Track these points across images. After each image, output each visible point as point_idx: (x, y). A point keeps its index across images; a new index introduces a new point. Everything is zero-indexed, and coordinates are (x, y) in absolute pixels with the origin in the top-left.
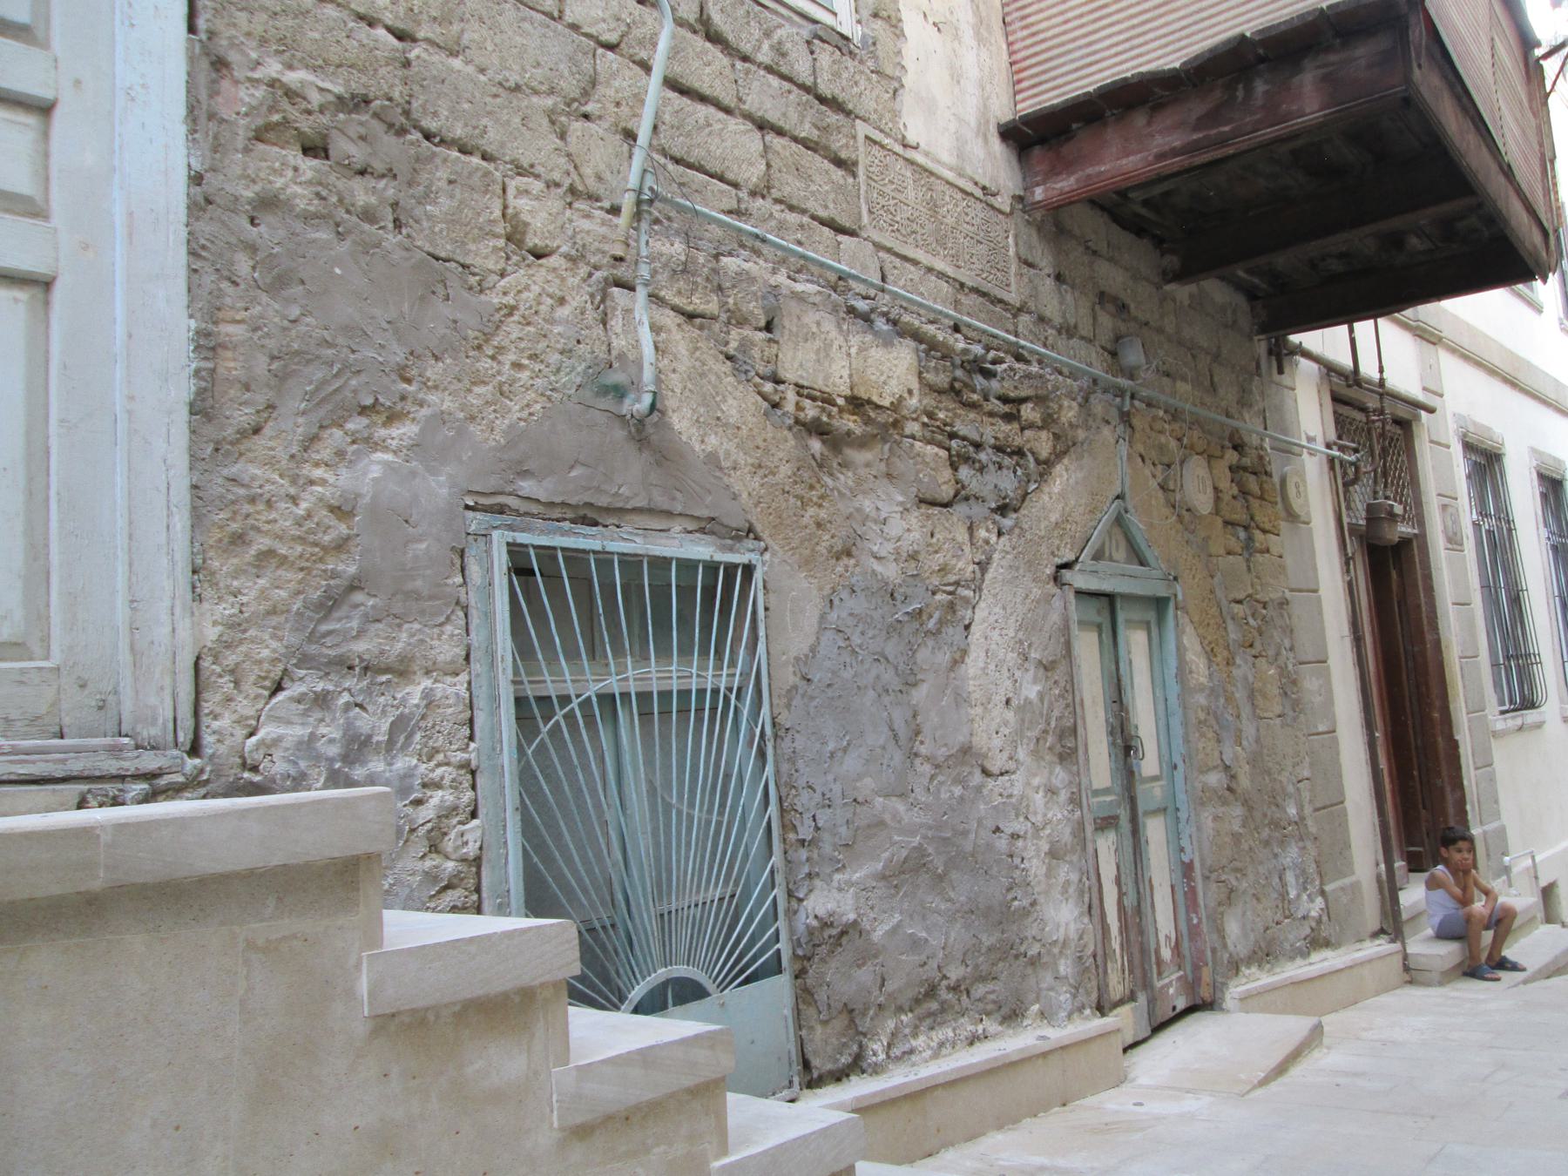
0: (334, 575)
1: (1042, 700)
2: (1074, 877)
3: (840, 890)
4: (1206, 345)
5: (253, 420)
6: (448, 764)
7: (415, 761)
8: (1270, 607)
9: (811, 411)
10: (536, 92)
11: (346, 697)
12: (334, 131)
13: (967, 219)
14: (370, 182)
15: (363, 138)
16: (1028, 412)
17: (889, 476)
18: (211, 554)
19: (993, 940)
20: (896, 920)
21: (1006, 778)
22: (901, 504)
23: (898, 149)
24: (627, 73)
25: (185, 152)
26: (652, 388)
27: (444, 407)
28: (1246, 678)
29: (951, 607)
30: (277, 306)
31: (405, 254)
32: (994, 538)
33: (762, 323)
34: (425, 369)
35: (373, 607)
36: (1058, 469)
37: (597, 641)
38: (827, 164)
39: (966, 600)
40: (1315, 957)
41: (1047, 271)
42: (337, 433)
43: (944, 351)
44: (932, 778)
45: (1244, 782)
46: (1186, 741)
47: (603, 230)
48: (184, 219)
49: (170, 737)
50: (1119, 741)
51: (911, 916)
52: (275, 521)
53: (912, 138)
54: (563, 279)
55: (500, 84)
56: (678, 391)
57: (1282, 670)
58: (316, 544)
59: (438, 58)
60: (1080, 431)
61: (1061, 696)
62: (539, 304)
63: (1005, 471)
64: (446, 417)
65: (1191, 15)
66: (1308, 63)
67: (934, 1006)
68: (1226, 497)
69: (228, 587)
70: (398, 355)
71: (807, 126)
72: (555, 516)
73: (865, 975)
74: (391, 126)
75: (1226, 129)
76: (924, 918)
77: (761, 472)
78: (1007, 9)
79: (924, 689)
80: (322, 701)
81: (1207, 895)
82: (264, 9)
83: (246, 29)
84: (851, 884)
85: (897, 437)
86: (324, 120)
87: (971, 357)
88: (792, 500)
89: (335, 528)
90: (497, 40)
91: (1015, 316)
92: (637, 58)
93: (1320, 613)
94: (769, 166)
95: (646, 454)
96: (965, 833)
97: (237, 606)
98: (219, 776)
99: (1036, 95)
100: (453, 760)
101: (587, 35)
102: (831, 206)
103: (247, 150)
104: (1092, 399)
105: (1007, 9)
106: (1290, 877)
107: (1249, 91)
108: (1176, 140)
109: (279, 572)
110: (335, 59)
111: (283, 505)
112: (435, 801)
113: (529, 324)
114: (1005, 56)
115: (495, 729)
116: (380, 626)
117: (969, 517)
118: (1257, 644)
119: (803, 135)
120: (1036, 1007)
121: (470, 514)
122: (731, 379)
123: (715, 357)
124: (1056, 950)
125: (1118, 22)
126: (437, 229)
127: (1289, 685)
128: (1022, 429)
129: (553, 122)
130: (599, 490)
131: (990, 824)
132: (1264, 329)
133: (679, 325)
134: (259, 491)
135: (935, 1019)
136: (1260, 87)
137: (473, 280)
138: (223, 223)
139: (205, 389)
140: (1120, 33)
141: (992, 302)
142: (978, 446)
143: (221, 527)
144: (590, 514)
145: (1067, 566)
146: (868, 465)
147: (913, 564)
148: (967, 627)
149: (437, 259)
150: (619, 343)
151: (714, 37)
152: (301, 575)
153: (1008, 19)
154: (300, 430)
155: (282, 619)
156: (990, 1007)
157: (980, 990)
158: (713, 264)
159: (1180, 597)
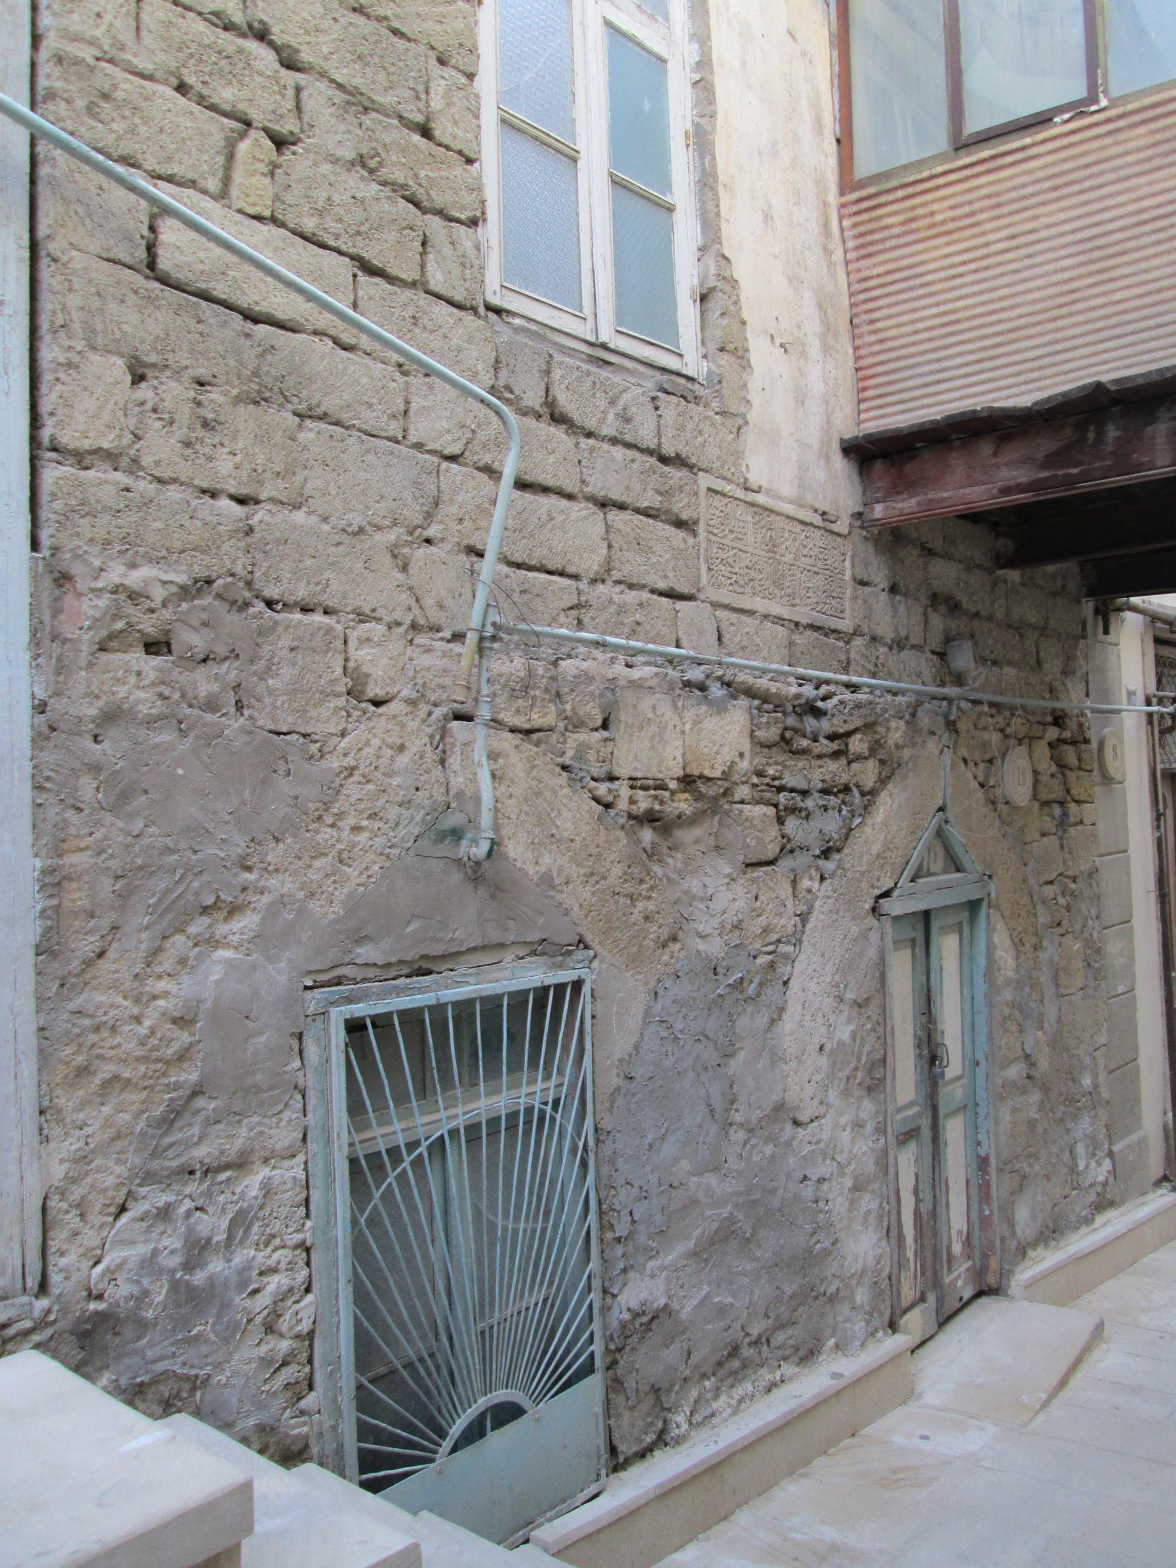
0: (177, 1086)
1: (854, 1039)
2: (874, 1205)
3: (652, 1276)
4: (1033, 620)
5: (97, 947)
6: (284, 1247)
7: (253, 1252)
8: (1080, 880)
9: (644, 802)
10: (379, 528)
11: (188, 1204)
12: (177, 624)
13: (805, 552)
14: (213, 668)
15: (205, 624)
16: (857, 744)
17: (717, 848)
18: (58, 1091)
19: (794, 1287)
20: (703, 1293)
21: (815, 1124)
22: (728, 875)
23: (740, 494)
24: (471, 484)
25: (28, 681)
26: (491, 834)
27: (285, 890)
28: (1052, 961)
29: (772, 966)
30: (120, 824)
31: (247, 738)
32: (816, 885)
33: (599, 723)
34: (267, 854)
35: (214, 1110)
36: (884, 795)
37: (428, 1081)
38: (670, 530)
39: (786, 956)
40: (1100, 1220)
41: (881, 586)
42: (179, 939)
43: (777, 702)
44: (746, 1143)
45: (1044, 1065)
46: (990, 1038)
47: (443, 663)
48: (28, 753)
49: (19, 1285)
50: (926, 1052)
51: (719, 1286)
52: (120, 1045)
53: (754, 479)
54: (403, 725)
55: (343, 530)
56: (514, 817)
57: (1089, 943)
58: (159, 1060)
59: (284, 515)
60: (906, 750)
61: (874, 1030)
62: (379, 757)
63: (830, 812)
64: (286, 899)
65: (1045, 345)
66: (1163, 413)
67: (735, 1364)
68: (1044, 779)
69: (73, 1122)
70: (239, 844)
71: (650, 493)
72: (390, 976)
73: (673, 1353)
74: (233, 603)
75: (1075, 471)
76: (731, 1283)
77: (592, 880)
78: (855, 310)
79: (741, 1056)
80: (165, 1213)
81: (999, 1187)
82: (106, 509)
83: (90, 536)
84: (662, 1268)
85: (726, 807)
86: (166, 614)
87: (803, 701)
88: (622, 900)
89: (178, 1039)
90: (341, 482)
91: (847, 643)
92: (481, 464)
93: (1128, 873)
94: (610, 546)
95: (482, 892)
96: (773, 1191)
97: (83, 1140)
98: (66, 1314)
99: (880, 407)
100: (289, 1243)
101: (430, 452)
102: (671, 574)
103: (91, 666)
104: (920, 713)
105: (855, 310)
106: (1080, 1150)
107: (1100, 433)
108: (1022, 475)
109: (123, 1096)
110: (178, 545)
111: (127, 1028)
112: (271, 1288)
113: (368, 781)
114: (851, 363)
115: (330, 1204)
116: (221, 1126)
117: (793, 870)
118: (1065, 923)
119: (646, 504)
120: (831, 1342)
121: (309, 995)
122: (567, 790)
123: (552, 772)
124: (853, 1282)
125: (969, 341)
126: (279, 703)
127: (1094, 951)
128: (849, 763)
129: (395, 556)
130: (435, 940)
131: (798, 1175)
132: (1092, 592)
133: (517, 747)
134: (104, 1018)
135: (736, 1377)
136: (1112, 432)
137: (314, 748)
138: (68, 748)
139: (51, 928)
140: (971, 352)
141: (826, 635)
142: (805, 793)
143: (67, 1063)
144: (425, 965)
145: (886, 894)
146: (697, 842)
147: (737, 933)
148: (785, 983)
149: (278, 734)
150: (457, 781)
151: (558, 418)
152: (144, 1094)
153: (855, 321)
154: (143, 946)
155: (126, 1142)
156: (789, 1351)
157: (779, 1338)
158: (553, 672)
159: (993, 895)
